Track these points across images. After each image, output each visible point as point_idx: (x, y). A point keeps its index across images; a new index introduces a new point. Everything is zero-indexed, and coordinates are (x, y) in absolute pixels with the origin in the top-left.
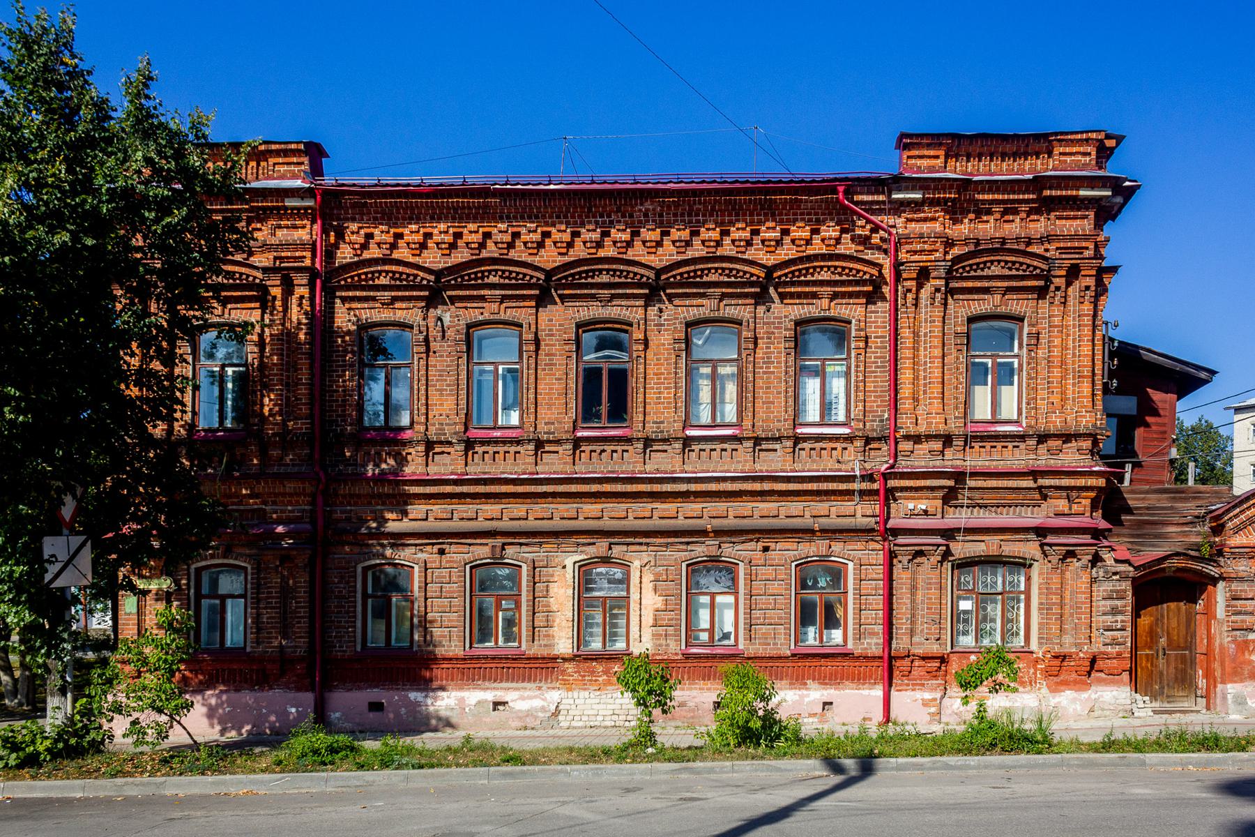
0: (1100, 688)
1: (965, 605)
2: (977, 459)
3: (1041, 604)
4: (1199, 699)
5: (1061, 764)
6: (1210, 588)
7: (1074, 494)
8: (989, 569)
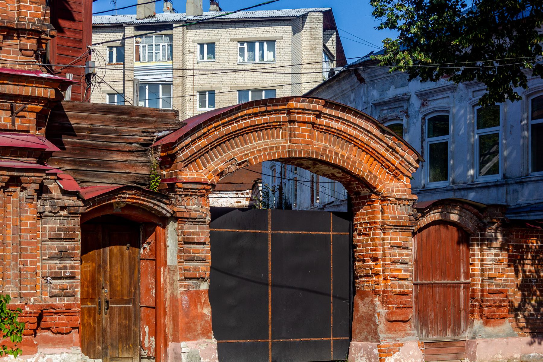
0: (48, 350)
6: (159, 229)
7: (18, 106)
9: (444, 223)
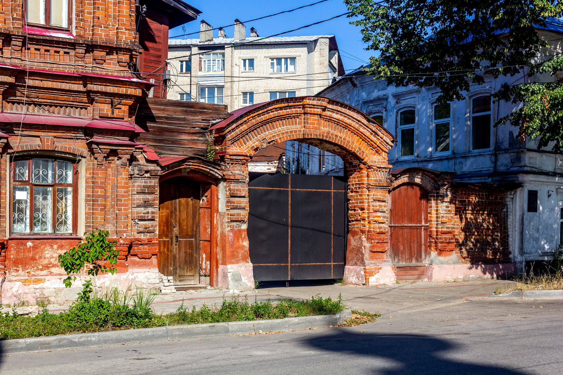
0: (135, 270)
1: (21, 195)
2: (32, 59)
3: (88, 196)
4: (203, 278)
5: (166, 335)
6: (213, 187)
7: (116, 101)
8: (41, 162)
9: (411, 184)
